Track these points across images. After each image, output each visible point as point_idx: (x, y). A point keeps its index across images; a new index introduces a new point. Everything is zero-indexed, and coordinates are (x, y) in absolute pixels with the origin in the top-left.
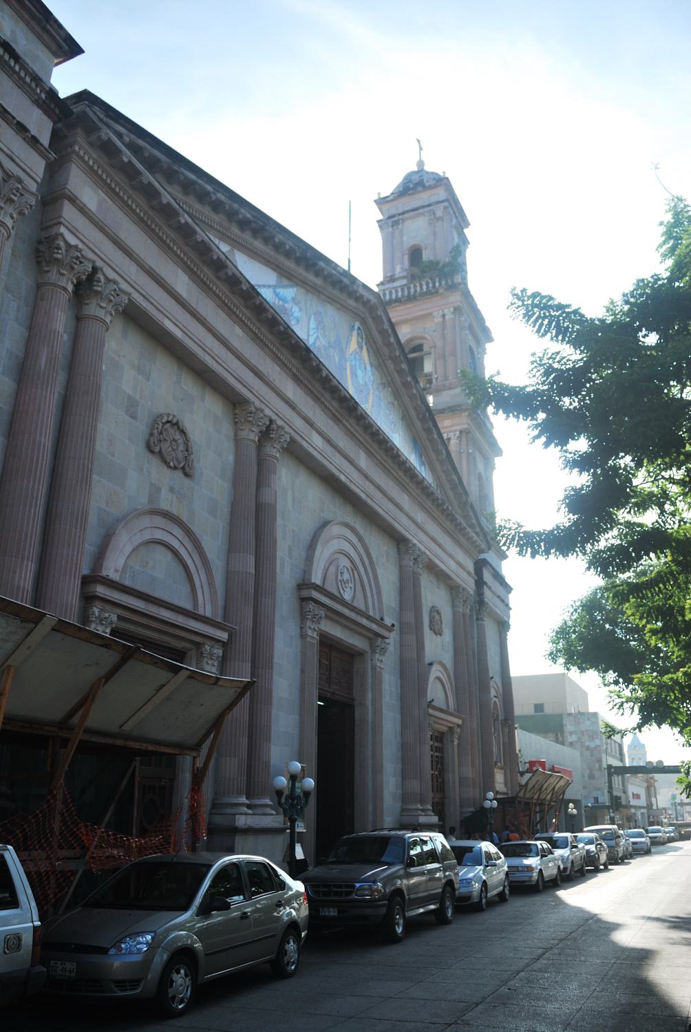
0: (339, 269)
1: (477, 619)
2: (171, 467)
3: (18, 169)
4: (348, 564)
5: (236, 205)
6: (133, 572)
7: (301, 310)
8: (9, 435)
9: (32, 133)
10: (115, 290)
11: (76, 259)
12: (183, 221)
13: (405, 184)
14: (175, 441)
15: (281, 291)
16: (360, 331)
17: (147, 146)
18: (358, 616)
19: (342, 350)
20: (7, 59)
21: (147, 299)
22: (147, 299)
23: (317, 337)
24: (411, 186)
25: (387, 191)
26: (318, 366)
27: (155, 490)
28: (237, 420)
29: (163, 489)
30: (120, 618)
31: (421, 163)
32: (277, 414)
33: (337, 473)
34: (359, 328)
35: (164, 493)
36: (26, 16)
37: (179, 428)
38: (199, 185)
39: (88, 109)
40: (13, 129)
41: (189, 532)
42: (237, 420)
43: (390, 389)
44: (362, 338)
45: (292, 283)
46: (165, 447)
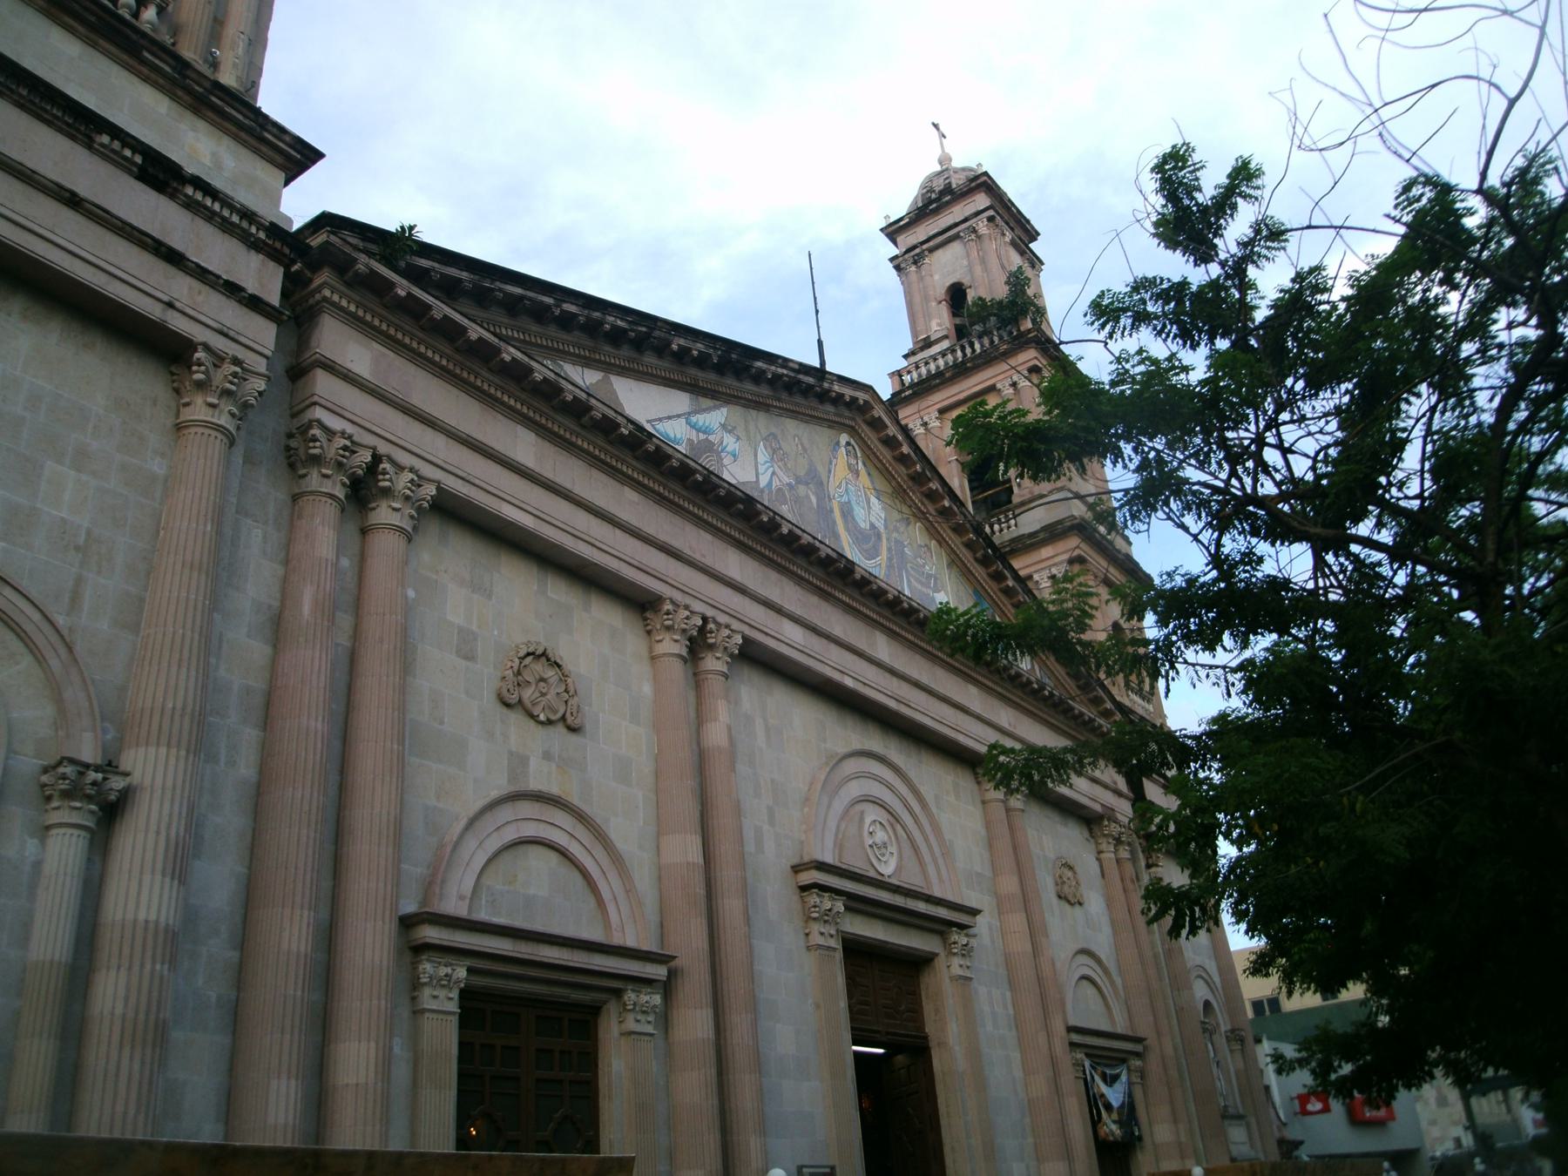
0: (791, 365)
1: (1149, 866)
2: (542, 723)
3: (233, 345)
4: (882, 816)
5: (597, 315)
6: (492, 894)
7: (738, 439)
8: (266, 724)
9: (250, 292)
10: (413, 480)
11: (344, 450)
12: (507, 358)
13: (923, 195)
14: (542, 680)
15: (701, 419)
16: (850, 448)
17: (436, 265)
18: (908, 899)
19: (822, 483)
20: (200, 199)
21: (468, 481)
22: (468, 481)
23: (774, 473)
24: (934, 196)
25: (900, 208)
26: (772, 520)
27: (518, 762)
28: (649, 628)
29: (532, 758)
30: (470, 970)
31: (944, 160)
32: (714, 607)
33: (836, 676)
34: (848, 444)
35: (534, 763)
36: (234, 129)
37: (548, 660)
38: (530, 299)
39: (332, 237)
40: (220, 291)
41: (580, 816)
42: (649, 628)
43: (918, 524)
44: (856, 457)
45: (718, 403)
46: (528, 694)
